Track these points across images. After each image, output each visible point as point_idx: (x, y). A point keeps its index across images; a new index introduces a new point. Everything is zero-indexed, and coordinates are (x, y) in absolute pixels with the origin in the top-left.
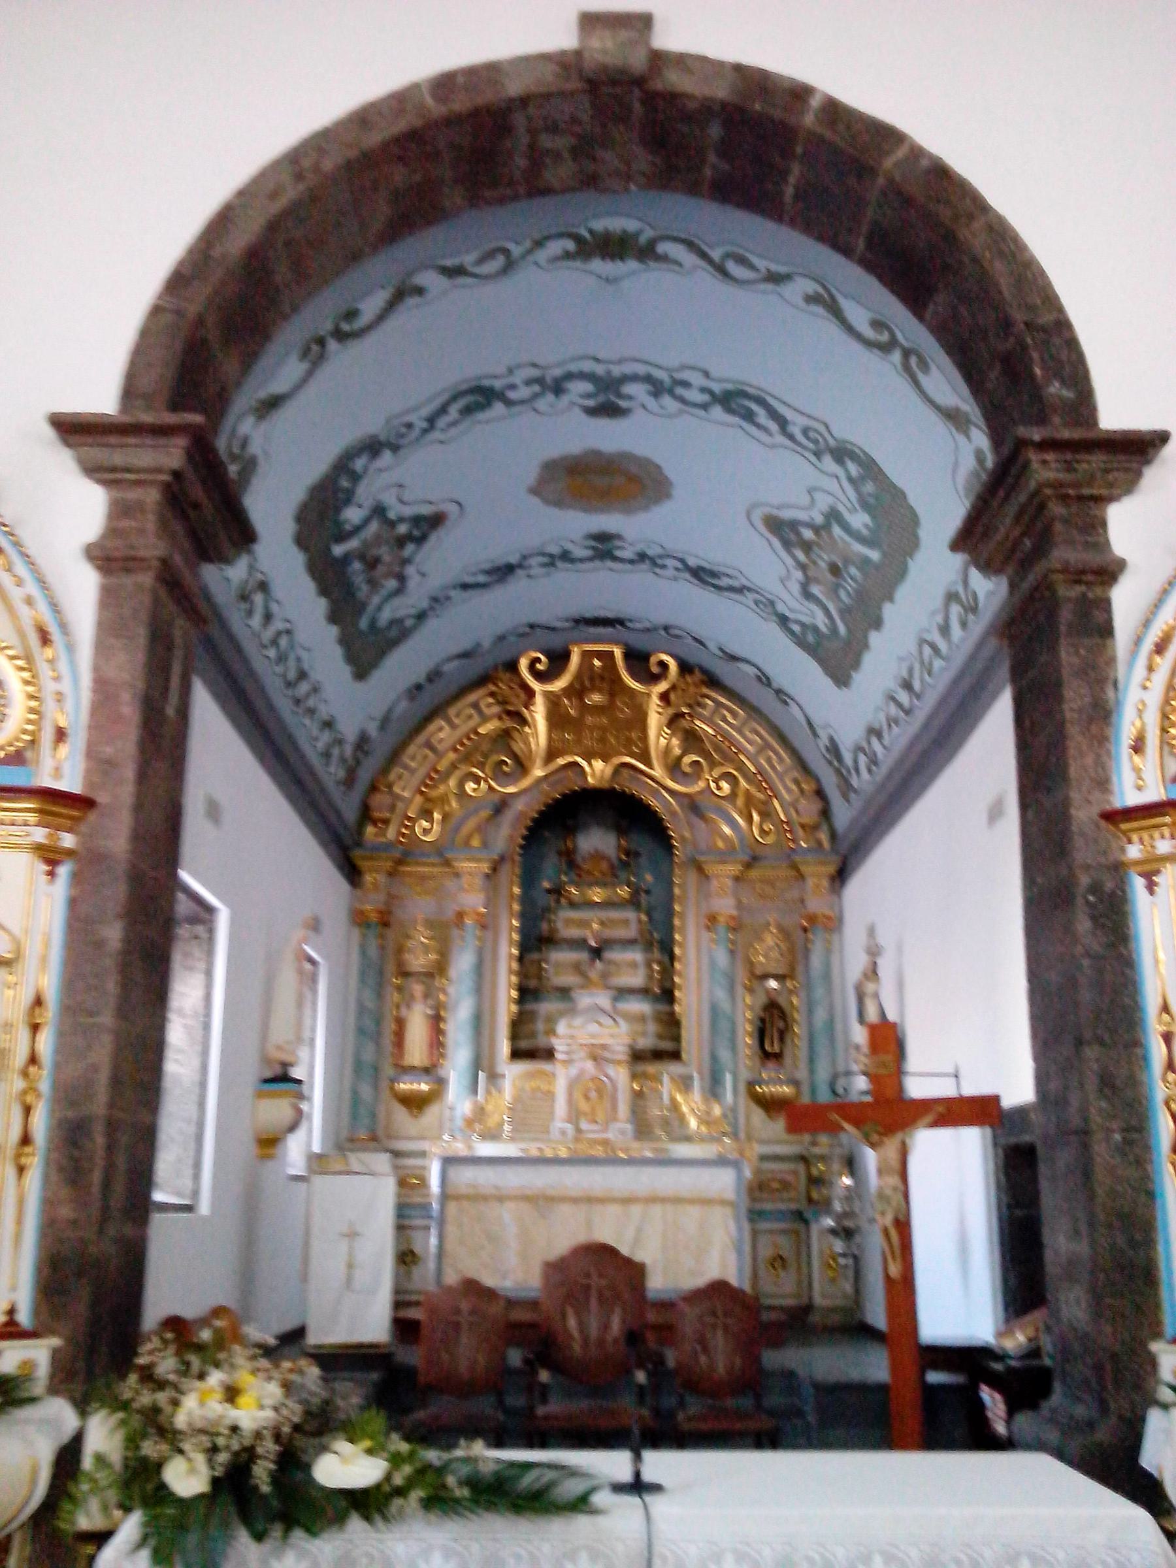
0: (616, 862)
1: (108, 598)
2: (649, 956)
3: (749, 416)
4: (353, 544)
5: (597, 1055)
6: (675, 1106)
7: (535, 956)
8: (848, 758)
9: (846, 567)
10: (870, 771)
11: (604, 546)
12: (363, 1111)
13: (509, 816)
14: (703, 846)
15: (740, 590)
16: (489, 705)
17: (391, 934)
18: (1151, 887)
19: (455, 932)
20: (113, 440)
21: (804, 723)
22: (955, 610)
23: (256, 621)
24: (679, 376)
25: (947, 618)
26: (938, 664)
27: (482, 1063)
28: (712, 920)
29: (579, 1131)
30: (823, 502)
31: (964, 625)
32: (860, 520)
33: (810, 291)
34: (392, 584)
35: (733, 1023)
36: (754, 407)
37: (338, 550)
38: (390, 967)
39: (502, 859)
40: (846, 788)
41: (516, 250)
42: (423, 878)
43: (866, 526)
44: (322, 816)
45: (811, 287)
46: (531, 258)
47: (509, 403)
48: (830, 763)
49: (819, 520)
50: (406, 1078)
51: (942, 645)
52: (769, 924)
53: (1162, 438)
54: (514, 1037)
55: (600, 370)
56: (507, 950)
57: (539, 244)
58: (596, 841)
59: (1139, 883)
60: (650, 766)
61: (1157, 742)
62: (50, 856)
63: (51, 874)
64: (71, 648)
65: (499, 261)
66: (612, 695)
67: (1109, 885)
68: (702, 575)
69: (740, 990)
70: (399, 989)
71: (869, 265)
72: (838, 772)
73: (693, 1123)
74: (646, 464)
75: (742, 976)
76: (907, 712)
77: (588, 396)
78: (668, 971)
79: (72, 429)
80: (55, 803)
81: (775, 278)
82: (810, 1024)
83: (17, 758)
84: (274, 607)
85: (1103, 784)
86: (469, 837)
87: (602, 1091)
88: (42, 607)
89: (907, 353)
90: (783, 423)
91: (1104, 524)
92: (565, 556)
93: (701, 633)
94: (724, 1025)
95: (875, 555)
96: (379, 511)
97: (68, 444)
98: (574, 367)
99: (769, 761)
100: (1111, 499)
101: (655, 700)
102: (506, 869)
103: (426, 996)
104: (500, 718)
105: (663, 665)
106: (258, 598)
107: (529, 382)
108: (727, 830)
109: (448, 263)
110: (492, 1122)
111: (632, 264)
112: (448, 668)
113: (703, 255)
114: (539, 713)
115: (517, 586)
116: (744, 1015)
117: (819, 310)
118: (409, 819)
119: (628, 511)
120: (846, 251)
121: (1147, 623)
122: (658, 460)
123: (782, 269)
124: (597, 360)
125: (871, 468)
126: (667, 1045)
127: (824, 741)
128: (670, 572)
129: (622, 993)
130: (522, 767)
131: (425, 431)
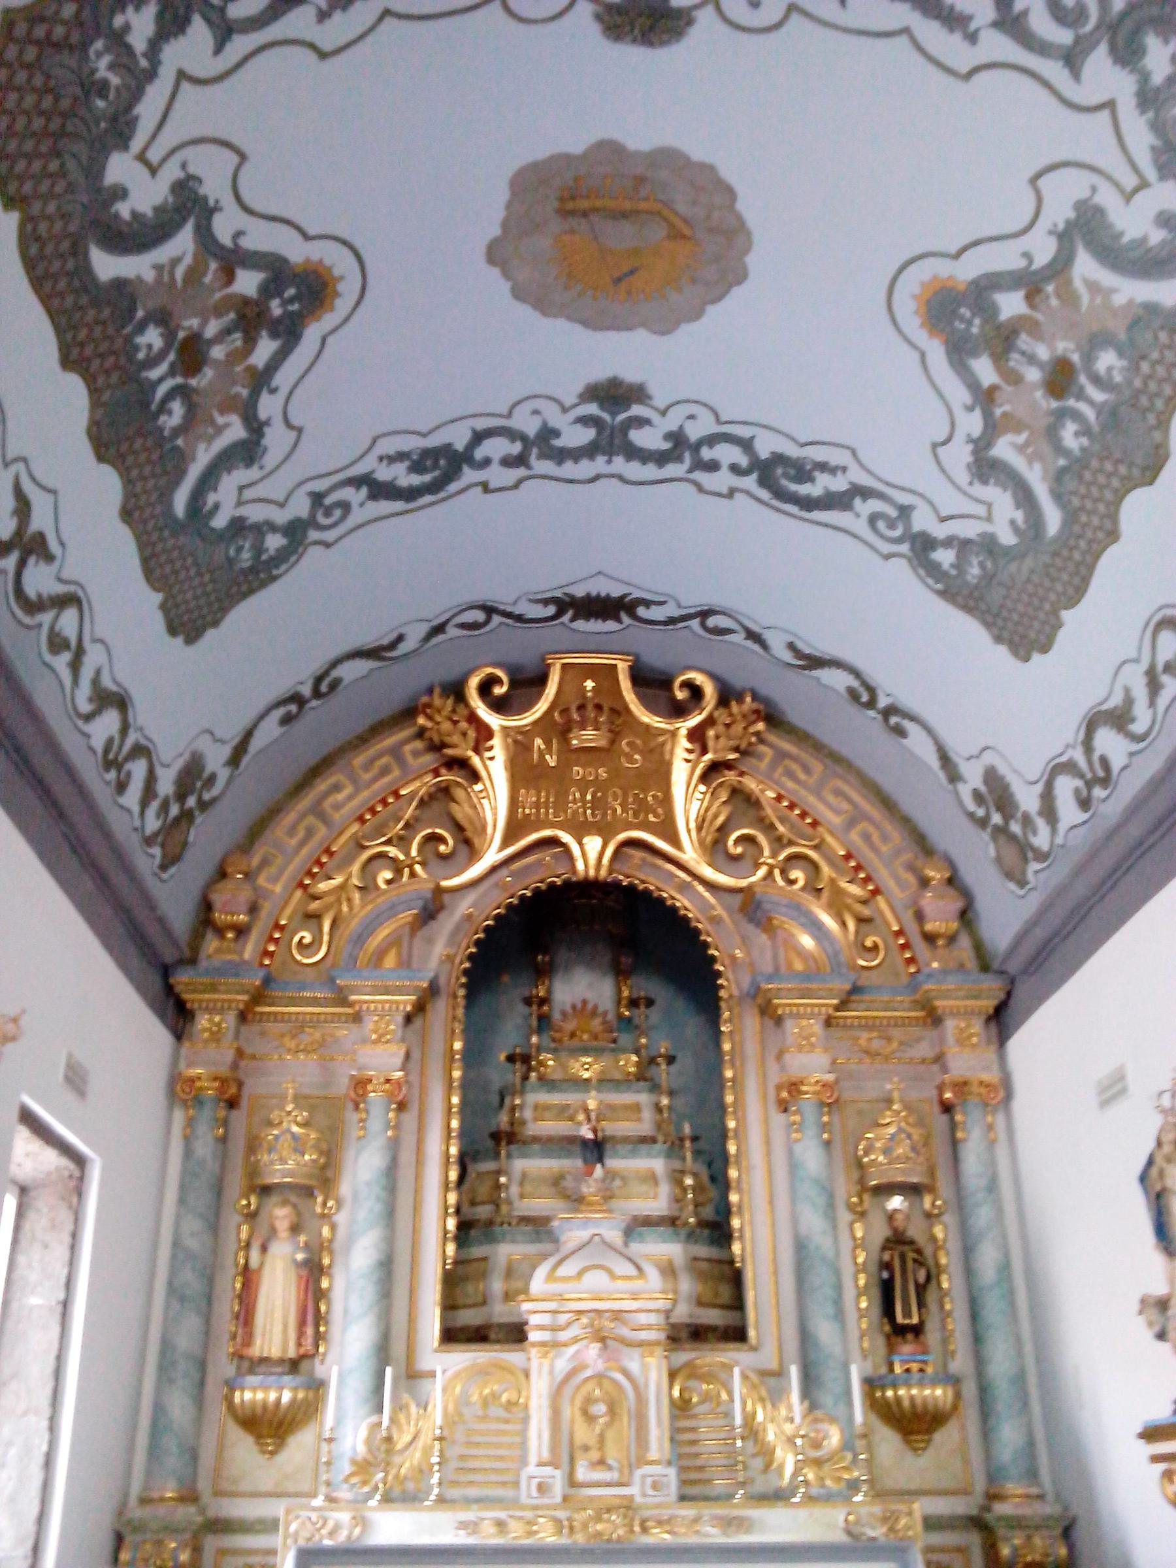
0: (611, 1017)
2: (677, 1165)
5: (605, 1331)
6: (752, 1431)
7: (489, 1166)
8: (1028, 799)
9: (1089, 358)
10: (1085, 803)
12: (170, 1443)
13: (447, 923)
14: (767, 967)
16: (416, 754)
17: (238, 1118)
19: (353, 1117)
21: (933, 761)
23: (132, 797)
27: (391, 1354)
28: (789, 1095)
29: (572, 1482)
34: (235, 431)
35: (837, 1273)
38: (236, 1180)
39: (433, 990)
40: (1016, 854)
42: (301, 1025)
44: (121, 909)
48: (983, 823)
50: (252, 1380)
52: (889, 1101)
54: (449, 1305)
56: (438, 1149)
58: (582, 988)
60: (675, 842)
66: (615, 736)
68: (781, 478)
69: (844, 1216)
70: (252, 1217)
73: (788, 1461)
75: (844, 1188)
78: (719, 1180)
82: (969, 1272)
86: (380, 954)
87: (615, 1404)
93: (760, 616)
94: (820, 1277)
96: (188, 204)
99: (866, 837)
101: (683, 743)
102: (440, 1010)
103: (295, 1229)
104: (436, 773)
105: (696, 692)
108: (807, 941)
110: (407, 1464)
114: (495, 766)
115: (461, 512)
116: (850, 1254)
118: (281, 928)
119: (665, 327)
122: (729, 173)
126: (713, 1317)
127: (973, 777)
128: (722, 480)
129: (638, 1225)
130: (469, 846)
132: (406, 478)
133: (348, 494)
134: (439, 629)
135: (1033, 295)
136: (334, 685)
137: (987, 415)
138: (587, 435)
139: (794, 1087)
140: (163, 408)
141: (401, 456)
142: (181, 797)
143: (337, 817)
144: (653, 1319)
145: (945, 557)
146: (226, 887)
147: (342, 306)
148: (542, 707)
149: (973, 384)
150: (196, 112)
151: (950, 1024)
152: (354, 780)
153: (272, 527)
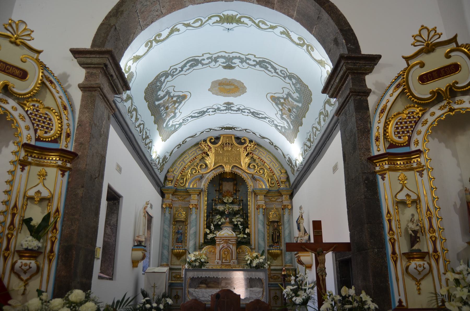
1: (83, 99)
3: (266, 68)
4: (161, 101)
11: (229, 106)
15: (265, 118)
16: (199, 151)
18: (383, 178)
20: (88, 56)
22: (322, 117)
23: (134, 119)
24: (247, 57)
25: (320, 120)
26: (318, 132)
30: (286, 91)
31: (324, 120)
32: (296, 95)
33: (282, 31)
34: (172, 114)
36: (267, 65)
37: (157, 103)
41: (204, 20)
43: (297, 97)
45: (282, 29)
46: (207, 22)
47: (203, 65)
48: (289, 165)
49: (285, 96)
51: (319, 127)
53: (379, 57)
55: (227, 55)
57: (210, 18)
59: (380, 177)
61: (383, 138)
62: (63, 170)
63: (63, 175)
64: (73, 111)
65: (199, 24)
67: (371, 179)
68: (255, 114)
71: (297, 20)
72: (291, 167)
74: (239, 82)
76: (310, 148)
77: (223, 63)
79: (76, 53)
80: (65, 154)
81: (272, 28)
83: (55, 141)
84: (139, 116)
85: (368, 149)
88: (64, 99)
89: (308, 46)
90: (275, 69)
91: (365, 80)
92: (218, 109)
95: (300, 105)
96: (168, 93)
97: (76, 58)
98: (220, 54)
99: (273, 165)
100: (367, 74)
106: (134, 113)
107: (208, 59)
109: (186, 22)
111: (235, 25)
112: (187, 140)
113: (254, 22)
115: (206, 118)
117: (284, 36)
120: (291, 16)
121: (378, 105)
123: (274, 25)
124: (226, 53)
125: (299, 80)
127: (287, 159)
128: (246, 114)
131: (180, 71)
132: (196, 115)
133: (188, 118)
134: (203, 132)
135: (284, 100)
136: (185, 142)
137: (282, 112)
138: (234, 61)
139: (259, 206)
140: (163, 115)
141: (196, 113)
142: (163, 162)
143: (186, 162)
144: (234, 240)
145: (280, 128)
146: (169, 174)
147: (187, 98)
148: (220, 143)
149: (279, 108)
150: (169, 84)
151: (284, 196)
152: (189, 155)
153: (177, 124)
